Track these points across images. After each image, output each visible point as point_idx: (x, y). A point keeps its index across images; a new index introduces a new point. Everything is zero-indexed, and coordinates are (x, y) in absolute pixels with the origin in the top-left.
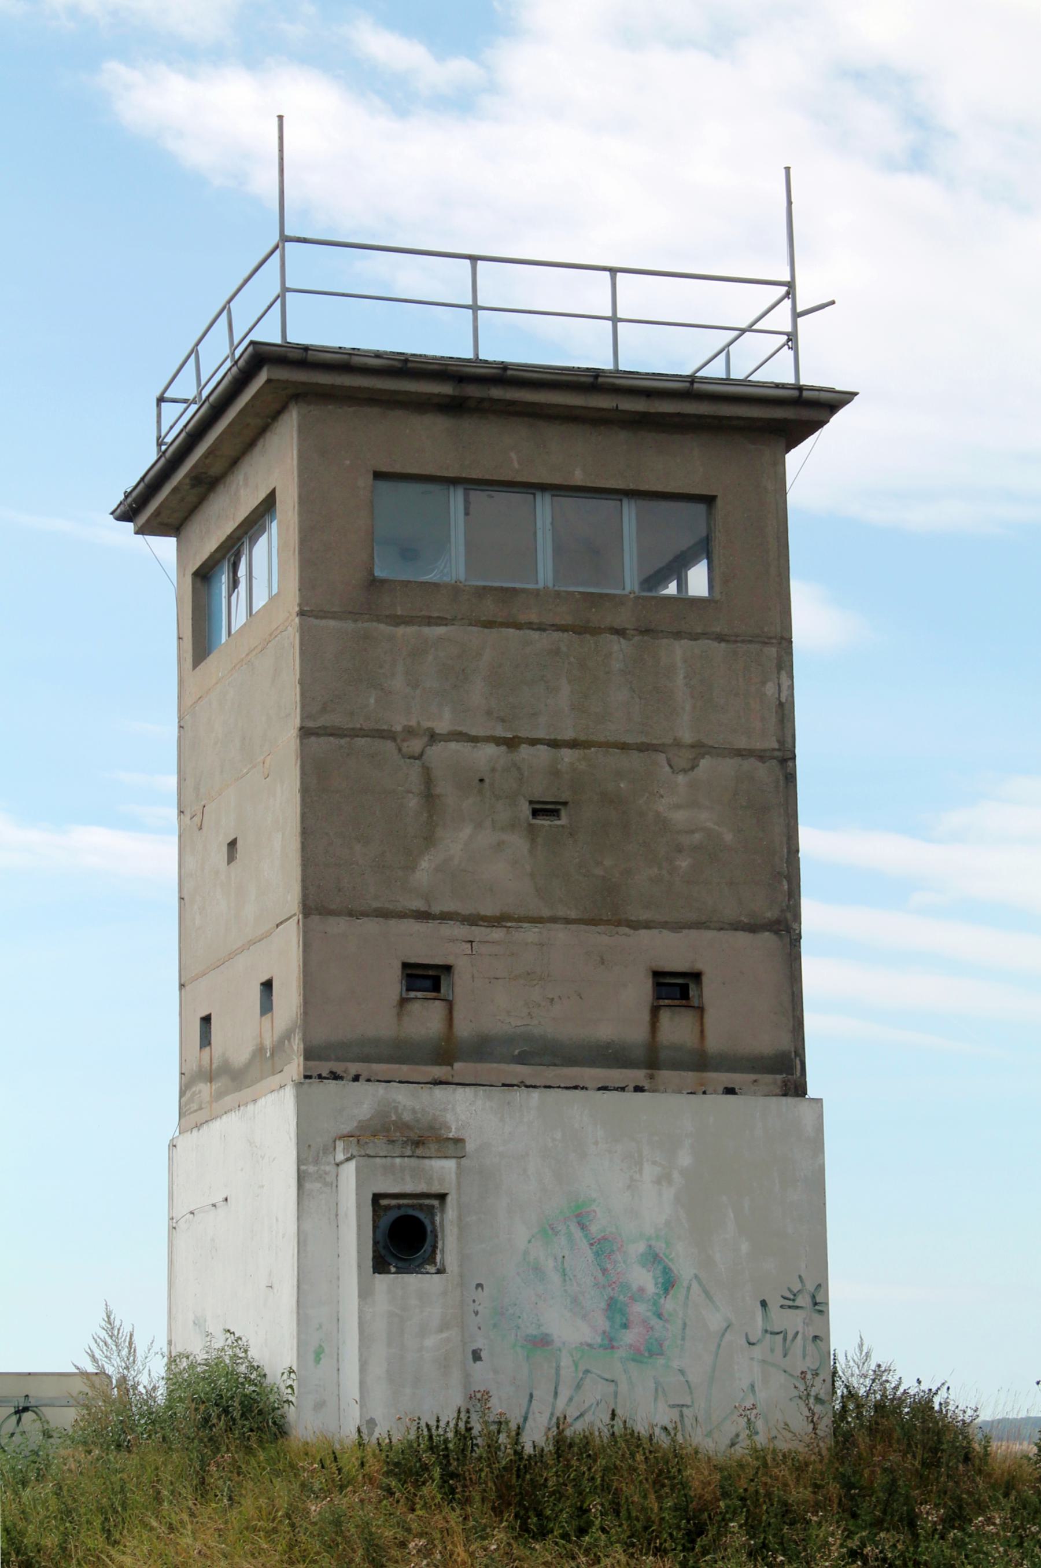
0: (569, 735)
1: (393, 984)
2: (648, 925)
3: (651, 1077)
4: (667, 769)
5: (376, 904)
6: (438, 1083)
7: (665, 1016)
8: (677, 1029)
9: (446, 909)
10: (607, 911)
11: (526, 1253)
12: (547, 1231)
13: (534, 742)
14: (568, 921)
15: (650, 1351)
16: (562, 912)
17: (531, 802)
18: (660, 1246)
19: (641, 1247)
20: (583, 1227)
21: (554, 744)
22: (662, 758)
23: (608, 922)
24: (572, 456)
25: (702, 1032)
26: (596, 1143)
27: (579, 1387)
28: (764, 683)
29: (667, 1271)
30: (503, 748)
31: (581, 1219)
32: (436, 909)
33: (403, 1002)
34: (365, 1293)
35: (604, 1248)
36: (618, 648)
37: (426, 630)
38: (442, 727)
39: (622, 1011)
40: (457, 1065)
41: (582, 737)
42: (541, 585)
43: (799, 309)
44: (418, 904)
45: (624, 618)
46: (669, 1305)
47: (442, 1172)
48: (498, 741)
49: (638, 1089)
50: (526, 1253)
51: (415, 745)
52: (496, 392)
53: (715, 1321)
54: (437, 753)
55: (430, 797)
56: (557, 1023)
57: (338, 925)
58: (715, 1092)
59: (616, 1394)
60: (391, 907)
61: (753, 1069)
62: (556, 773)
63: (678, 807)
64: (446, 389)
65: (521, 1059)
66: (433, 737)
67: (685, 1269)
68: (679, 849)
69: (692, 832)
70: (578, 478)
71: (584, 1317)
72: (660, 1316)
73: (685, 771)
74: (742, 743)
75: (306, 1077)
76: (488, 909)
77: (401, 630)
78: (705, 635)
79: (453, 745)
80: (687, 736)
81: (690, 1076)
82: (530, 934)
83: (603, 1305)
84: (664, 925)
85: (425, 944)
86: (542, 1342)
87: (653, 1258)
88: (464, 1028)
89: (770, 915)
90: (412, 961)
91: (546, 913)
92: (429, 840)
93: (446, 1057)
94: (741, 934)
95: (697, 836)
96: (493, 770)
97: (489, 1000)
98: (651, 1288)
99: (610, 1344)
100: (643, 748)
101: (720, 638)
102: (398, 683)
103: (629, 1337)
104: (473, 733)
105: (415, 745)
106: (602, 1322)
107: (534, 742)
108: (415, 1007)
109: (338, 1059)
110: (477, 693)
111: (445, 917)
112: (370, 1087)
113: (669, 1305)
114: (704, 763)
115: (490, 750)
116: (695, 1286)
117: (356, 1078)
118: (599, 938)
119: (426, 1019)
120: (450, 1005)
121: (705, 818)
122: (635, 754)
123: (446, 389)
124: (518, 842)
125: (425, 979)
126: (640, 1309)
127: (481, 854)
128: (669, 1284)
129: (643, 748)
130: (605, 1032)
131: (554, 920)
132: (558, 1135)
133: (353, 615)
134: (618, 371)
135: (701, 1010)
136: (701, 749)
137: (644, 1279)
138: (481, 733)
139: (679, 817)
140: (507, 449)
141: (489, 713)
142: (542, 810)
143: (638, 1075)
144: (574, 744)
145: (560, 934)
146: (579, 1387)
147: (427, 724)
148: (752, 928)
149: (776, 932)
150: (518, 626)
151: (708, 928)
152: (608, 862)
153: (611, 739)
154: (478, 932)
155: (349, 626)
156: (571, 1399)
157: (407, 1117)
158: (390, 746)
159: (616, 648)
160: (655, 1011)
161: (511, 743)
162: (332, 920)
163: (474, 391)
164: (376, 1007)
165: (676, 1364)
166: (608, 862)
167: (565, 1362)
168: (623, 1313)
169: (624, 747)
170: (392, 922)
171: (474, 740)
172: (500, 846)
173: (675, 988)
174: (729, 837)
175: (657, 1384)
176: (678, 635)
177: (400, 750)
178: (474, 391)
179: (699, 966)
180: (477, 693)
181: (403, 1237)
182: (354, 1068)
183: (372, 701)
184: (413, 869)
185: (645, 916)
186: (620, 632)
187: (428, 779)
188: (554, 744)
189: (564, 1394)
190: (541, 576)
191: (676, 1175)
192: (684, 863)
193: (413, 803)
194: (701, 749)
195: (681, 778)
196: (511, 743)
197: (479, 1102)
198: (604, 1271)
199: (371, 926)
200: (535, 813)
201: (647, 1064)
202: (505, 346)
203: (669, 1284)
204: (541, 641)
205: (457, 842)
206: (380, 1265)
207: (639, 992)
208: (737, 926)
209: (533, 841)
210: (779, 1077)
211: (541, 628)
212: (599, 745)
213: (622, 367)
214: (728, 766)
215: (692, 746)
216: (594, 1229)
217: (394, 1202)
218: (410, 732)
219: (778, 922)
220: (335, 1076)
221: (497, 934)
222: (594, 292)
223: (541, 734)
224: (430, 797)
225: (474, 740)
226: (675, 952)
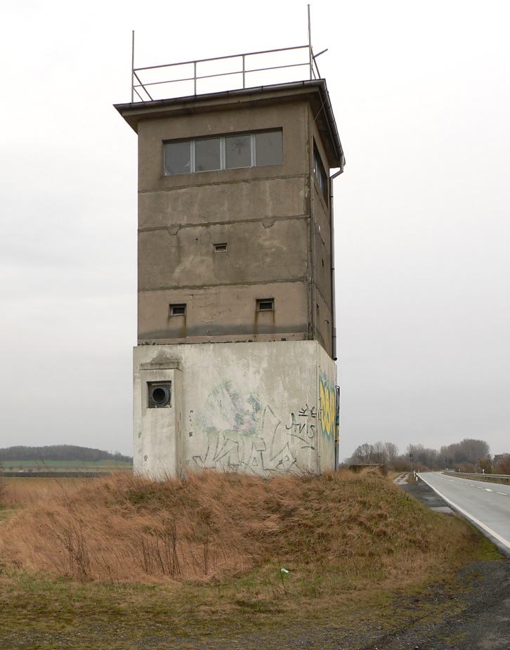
0: (227, 220)
1: (166, 311)
2: (255, 283)
3: (255, 337)
4: (262, 227)
5: (161, 286)
6: (181, 344)
7: (260, 315)
8: (265, 319)
9: (184, 284)
10: (240, 279)
11: (208, 400)
12: (215, 392)
13: (215, 224)
14: (226, 285)
15: (251, 432)
16: (224, 282)
17: (214, 245)
18: (255, 396)
19: (248, 396)
20: (228, 390)
21: (222, 223)
22: (261, 223)
23: (240, 284)
24: (231, 123)
25: (274, 320)
26: (233, 361)
27: (225, 445)
28: (299, 192)
29: (257, 404)
30: (204, 227)
31: (227, 386)
32: (181, 285)
33: (170, 317)
34: (144, 414)
35: (235, 397)
36: (245, 186)
37: (179, 191)
38: (184, 222)
39: (245, 313)
40: (187, 337)
41: (232, 220)
42: (221, 169)
43: (314, 55)
44: (175, 284)
45: (247, 176)
46: (257, 416)
47: (170, 374)
48: (202, 225)
49: (250, 341)
50: (208, 400)
51: (174, 230)
52: (197, 105)
53: (274, 421)
54: (182, 232)
55: (179, 248)
56: (223, 320)
57: (149, 294)
58: (278, 340)
59: (238, 447)
60: (166, 286)
61: (293, 331)
62: (222, 233)
63: (266, 240)
64: (180, 107)
65: (209, 334)
66: (181, 227)
67: (264, 403)
68: (266, 255)
69: (271, 248)
70: (232, 129)
71: (227, 421)
72: (254, 420)
73: (269, 227)
74: (291, 214)
75: (138, 345)
76: (198, 283)
77: (170, 192)
78: (277, 177)
79: (187, 229)
80: (270, 214)
81: (269, 335)
82: (213, 290)
83: (234, 417)
84: (261, 283)
85: (177, 297)
86: (212, 430)
87: (252, 400)
88: (190, 324)
89: (301, 275)
90: (172, 303)
91: (218, 282)
92: (179, 262)
93: (183, 336)
94: (289, 283)
95: (273, 250)
96: (201, 235)
97: (198, 315)
98: (251, 410)
99: (236, 429)
100: (253, 221)
101: (283, 177)
102: (169, 210)
103: (243, 427)
104: (194, 223)
105: (174, 230)
106: (234, 423)
107: (215, 224)
108: (174, 319)
109: (148, 339)
110: (196, 210)
111: (183, 287)
112: (155, 347)
113: (257, 416)
114: (276, 223)
115: (200, 228)
116: (267, 408)
117: (154, 344)
118: (238, 289)
119: (177, 322)
120: (185, 317)
121: (276, 242)
122: (251, 223)
123: (180, 107)
124: (209, 259)
125: (178, 309)
126: (247, 418)
127: (197, 264)
128: (258, 408)
129: (253, 221)
130: (239, 322)
131: (221, 285)
132: (219, 359)
133: (155, 189)
134: (196, 95)
135: (274, 312)
136: (275, 218)
137: (249, 407)
138: (198, 223)
139: (267, 244)
140: (208, 125)
141: (200, 216)
142: (220, 246)
143: (250, 337)
144: (229, 223)
145: (223, 289)
146: (225, 445)
147: (178, 223)
148: (293, 281)
149: (303, 281)
150: (210, 185)
151: (277, 282)
152: (240, 263)
153: (243, 219)
154: (195, 292)
155: (153, 193)
156: (222, 449)
157: (168, 356)
158: (166, 232)
159: (245, 186)
160: (257, 313)
161: (207, 225)
162: (146, 292)
163: (189, 106)
164: (162, 318)
165: (259, 436)
166: (240, 263)
167: (221, 436)
168: (241, 419)
169: (247, 221)
170: (167, 291)
171: (195, 226)
172: (203, 261)
173: (265, 304)
174: (285, 249)
175: (253, 443)
176: (267, 178)
177: (169, 232)
178: (189, 106)
179: (273, 296)
180: (196, 210)
181: (158, 395)
182: (153, 341)
183: (161, 217)
184: (173, 273)
185: (253, 280)
186: (246, 181)
187: (179, 240)
188: (222, 223)
189: (220, 446)
190: (191, 170)
191: (261, 371)
192: (268, 260)
193: (174, 250)
194: (275, 218)
195: (268, 230)
196: (207, 225)
197: (192, 350)
198: (235, 405)
199: (159, 293)
200: (217, 248)
201: (252, 333)
202: (207, 87)
203: (258, 408)
204: (218, 188)
205: (188, 262)
206: (151, 405)
207: (251, 307)
208: (287, 281)
209: (214, 259)
210: (302, 333)
211: (218, 184)
212: (238, 222)
213: (197, 94)
214: (285, 223)
215: (272, 217)
216: (231, 390)
217: (156, 384)
218: (173, 226)
219: (303, 277)
220: (147, 344)
221: (202, 291)
222: (188, 71)
223: (217, 221)
224: (179, 248)
225: (195, 226)
226: (264, 292)
